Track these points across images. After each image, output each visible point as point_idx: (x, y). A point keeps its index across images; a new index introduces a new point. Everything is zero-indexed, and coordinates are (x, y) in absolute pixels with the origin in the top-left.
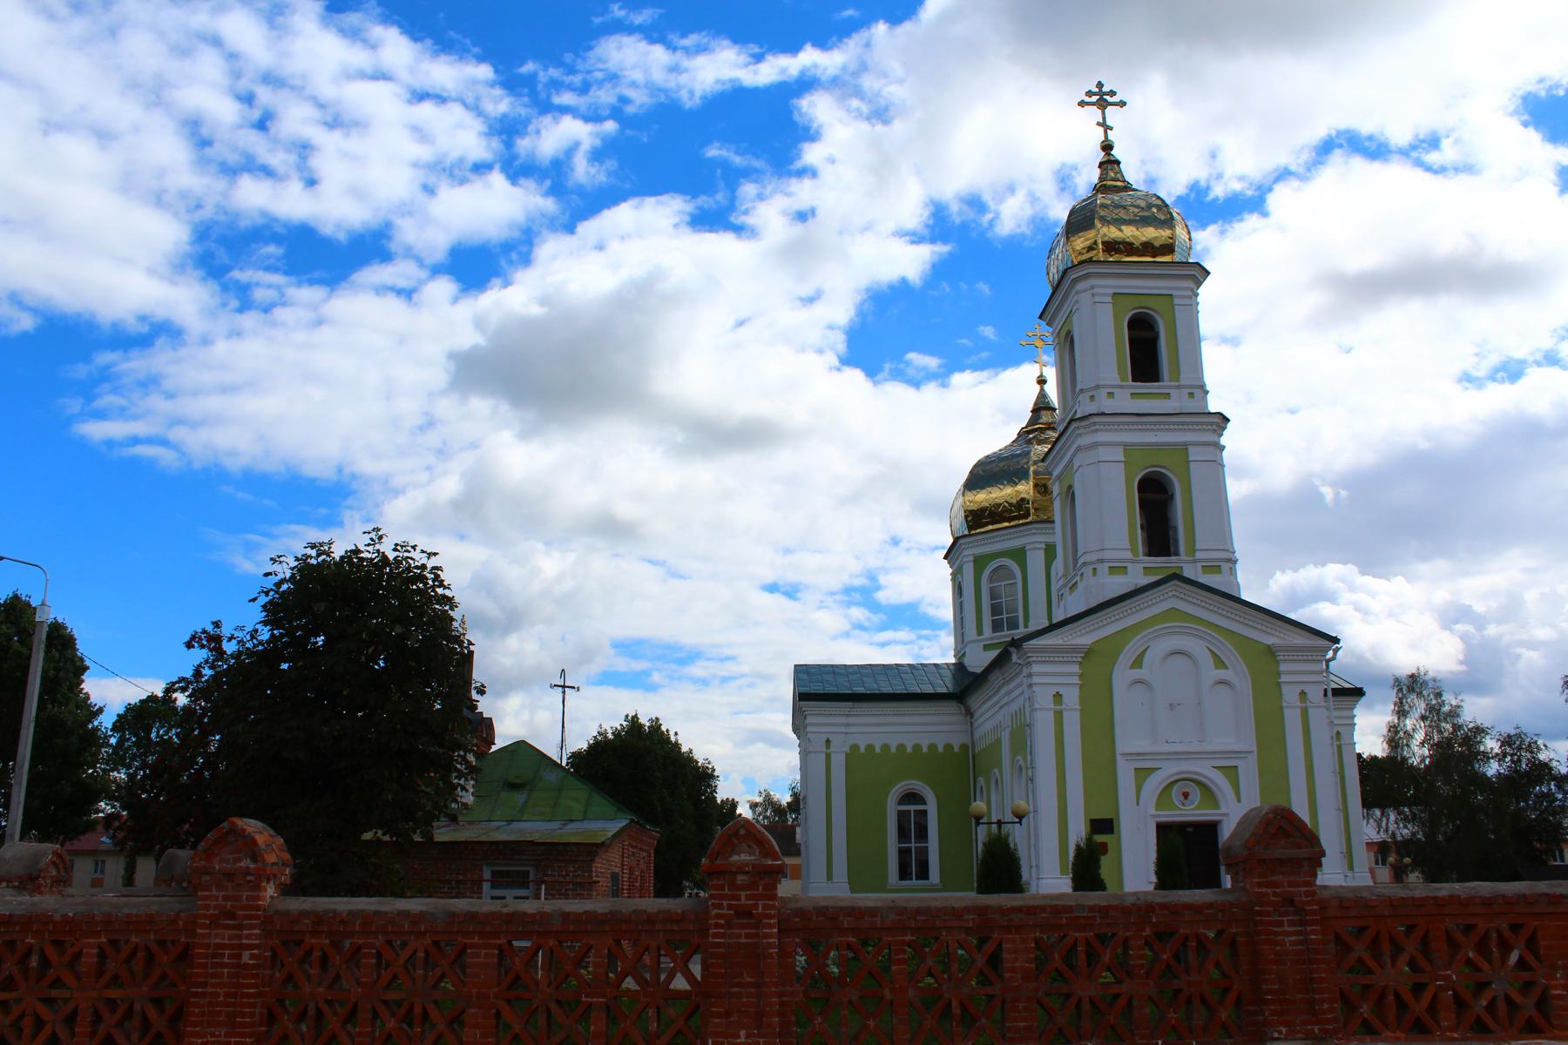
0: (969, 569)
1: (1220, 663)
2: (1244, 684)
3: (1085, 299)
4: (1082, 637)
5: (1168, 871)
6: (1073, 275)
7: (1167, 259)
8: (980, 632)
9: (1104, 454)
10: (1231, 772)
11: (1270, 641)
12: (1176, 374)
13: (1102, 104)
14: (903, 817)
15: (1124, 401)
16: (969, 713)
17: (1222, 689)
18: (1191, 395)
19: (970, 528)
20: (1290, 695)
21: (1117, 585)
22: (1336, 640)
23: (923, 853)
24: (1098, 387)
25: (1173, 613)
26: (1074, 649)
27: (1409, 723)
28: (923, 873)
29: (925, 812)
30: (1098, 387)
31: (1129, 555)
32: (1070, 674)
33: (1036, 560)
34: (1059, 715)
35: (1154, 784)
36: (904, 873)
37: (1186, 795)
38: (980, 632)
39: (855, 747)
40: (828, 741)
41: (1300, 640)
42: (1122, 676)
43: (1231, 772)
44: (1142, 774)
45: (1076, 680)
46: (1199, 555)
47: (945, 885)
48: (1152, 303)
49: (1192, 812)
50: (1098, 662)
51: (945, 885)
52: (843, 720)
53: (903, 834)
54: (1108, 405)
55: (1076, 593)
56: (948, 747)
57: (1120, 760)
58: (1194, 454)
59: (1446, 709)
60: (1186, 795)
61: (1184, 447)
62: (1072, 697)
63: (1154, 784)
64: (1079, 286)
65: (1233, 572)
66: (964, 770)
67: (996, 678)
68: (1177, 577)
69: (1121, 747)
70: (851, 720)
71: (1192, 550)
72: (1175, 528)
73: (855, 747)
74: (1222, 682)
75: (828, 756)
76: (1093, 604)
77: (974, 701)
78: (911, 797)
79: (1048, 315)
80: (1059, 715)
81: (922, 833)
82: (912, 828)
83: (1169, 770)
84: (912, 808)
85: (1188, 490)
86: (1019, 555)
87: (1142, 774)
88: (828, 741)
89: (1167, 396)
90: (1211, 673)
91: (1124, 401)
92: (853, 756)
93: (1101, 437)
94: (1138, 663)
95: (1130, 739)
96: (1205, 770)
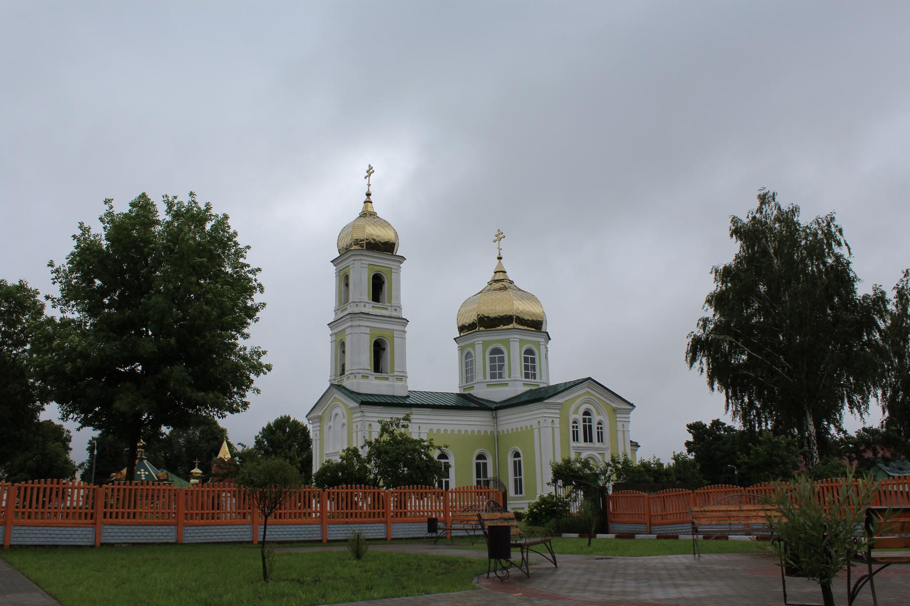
11: (614, 406)
33: (479, 348)
46: (395, 373)
58: (396, 334)
71: (393, 371)
86: (507, 343)
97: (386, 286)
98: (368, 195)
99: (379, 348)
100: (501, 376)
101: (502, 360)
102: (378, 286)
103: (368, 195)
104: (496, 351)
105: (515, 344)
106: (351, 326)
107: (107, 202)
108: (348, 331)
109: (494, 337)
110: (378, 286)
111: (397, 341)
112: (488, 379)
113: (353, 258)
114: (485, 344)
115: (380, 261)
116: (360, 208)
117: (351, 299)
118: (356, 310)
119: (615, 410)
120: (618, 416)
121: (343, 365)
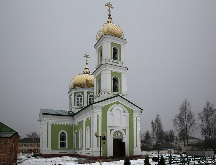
0: (73, 95)
1: (124, 112)
2: (128, 116)
3: (106, 42)
4: (104, 104)
6: (104, 36)
8: (75, 106)
9: (107, 71)
10: (125, 130)
14: (61, 137)
15: (111, 62)
16: (74, 119)
18: (122, 64)
19: (74, 87)
20: (135, 118)
21: (107, 96)
23: (65, 143)
24: (107, 59)
25: (118, 103)
28: (65, 146)
29: (65, 136)
30: (107, 59)
32: (100, 111)
33: (86, 94)
34: (98, 119)
35: (113, 132)
36: (61, 146)
37: (118, 134)
38: (75, 106)
39: (53, 124)
40: (48, 122)
42: (109, 112)
43: (125, 130)
44: (111, 130)
45: (101, 112)
47: (69, 148)
49: (118, 137)
50: (105, 110)
51: (69, 148)
52: (51, 119)
53: (61, 140)
54: (109, 62)
56: (70, 125)
57: (108, 127)
60: (118, 134)
62: (100, 115)
63: (113, 132)
64: (105, 39)
66: (73, 129)
68: (119, 95)
70: (52, 119)
72: (118, 87)
73: (53, 124)
75: (48, 125)
77: (75, 117)
78: (62, 133)
79: (95, 47)
80: (98, 119)
81: (65, 140)
82: (63, 138)
86: (83, 93)
87: (111, 130)
88: (48, 122)
89: (118, 63)
90: (123, 113)
91: (111, 62)
92: (52, 125)
93: (107, 68)
94: (111, 111)
95: (109, 123)
102: (115, 53)
104: (79, 96)
110: (115, 53)
115: (117, 41)
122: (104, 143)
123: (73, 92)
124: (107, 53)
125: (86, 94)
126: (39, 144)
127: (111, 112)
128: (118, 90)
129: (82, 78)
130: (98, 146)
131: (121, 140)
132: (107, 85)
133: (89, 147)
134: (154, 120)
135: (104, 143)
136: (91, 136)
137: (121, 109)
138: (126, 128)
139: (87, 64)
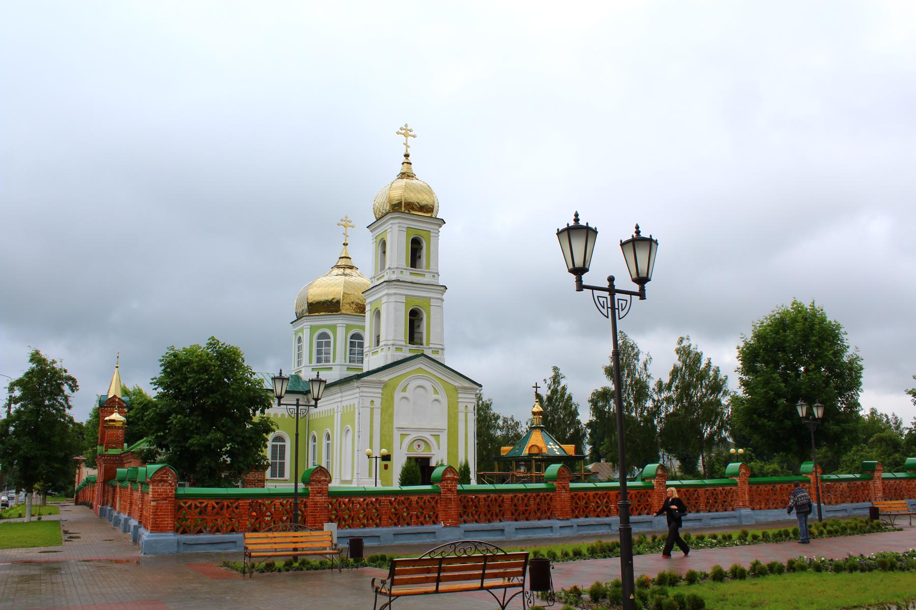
1: (436, 392)
4: (384, 377)
5: (406, 479)
7: (429, 215)
8: (310, 362)
10: (437, 437)
11: (456, 384)
12: (428, 266)
13: (406, 135)
17: (436, 403)
20: (461, 407)
22: (480, 386)
23: (282, 465)
26: (380, 382)
27: (775, 375)
28: (282, 474)
31: (404, 343)
33: (341, 332)
37: (419, 446)
38: (310, 362)
41: (467, 384)
42: (398, 395)
45: (380, 395)
46: (431, 346)
48: (423, 233)
49: (421, 453)
55: (375, 356)
57: (395, 431)
58: (433, 302)
59: (794, 511)
60: (419, 446)
61: (430, 298)
62: (378, 402)
65: (443, 354)
67: (336, 389)
68: (423, 355)
69: (395, 425)
71: (428, 344)
74: (436, 400)
76: (389, 362)
81: (282, 456)
83: (414, 435)
84: (278, 444)
85: (429, 317)
86: (334, 328)
94: (404, 390)
95: (400, 421)
96: (427, 435)
97: (424, 252)
98: (407, 156)
99: (414, 317)
100: (327, 361)
101: (328, 344)
102: (416, 249)
103: (407, 156)
104: (324, 336)
105: (339, 329)
106: (387, 294)
107: (406, 132)
108: (384, 300)
109: (323, 321)
110: (416, 249)
111: (433, 310)
112: (348, 363)
113: (391, 221)
114: (313, 329)
115: (419, 225)
116: (399, 169)
117: (387, 267)
118: (394, 277)
119: (456, 389)
120: (460, 395)
121: (378, 336)
122: (386, 467)
123: (306, 324)
124: (398, 252)
125: (341, 332)
126: (702, 506)
127: (404, 394)
128: (421, 339)
129: (328, 285)
130: (370, 475)
131: (427, 460)
132: (393, 326)
133: (348, 478)
134: (545, 392)
135: (386, 467)
136: (356, 449)
137: (428, 385)
138: (442, 430)
139: (345, 244)
